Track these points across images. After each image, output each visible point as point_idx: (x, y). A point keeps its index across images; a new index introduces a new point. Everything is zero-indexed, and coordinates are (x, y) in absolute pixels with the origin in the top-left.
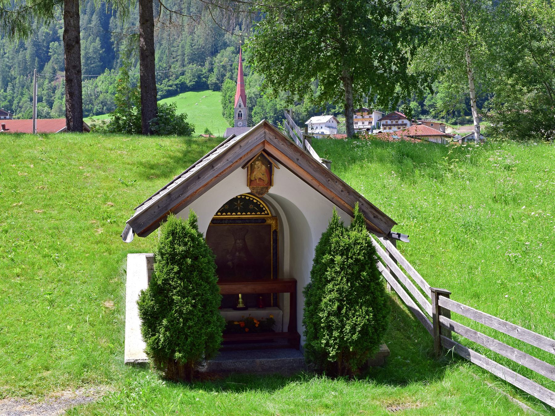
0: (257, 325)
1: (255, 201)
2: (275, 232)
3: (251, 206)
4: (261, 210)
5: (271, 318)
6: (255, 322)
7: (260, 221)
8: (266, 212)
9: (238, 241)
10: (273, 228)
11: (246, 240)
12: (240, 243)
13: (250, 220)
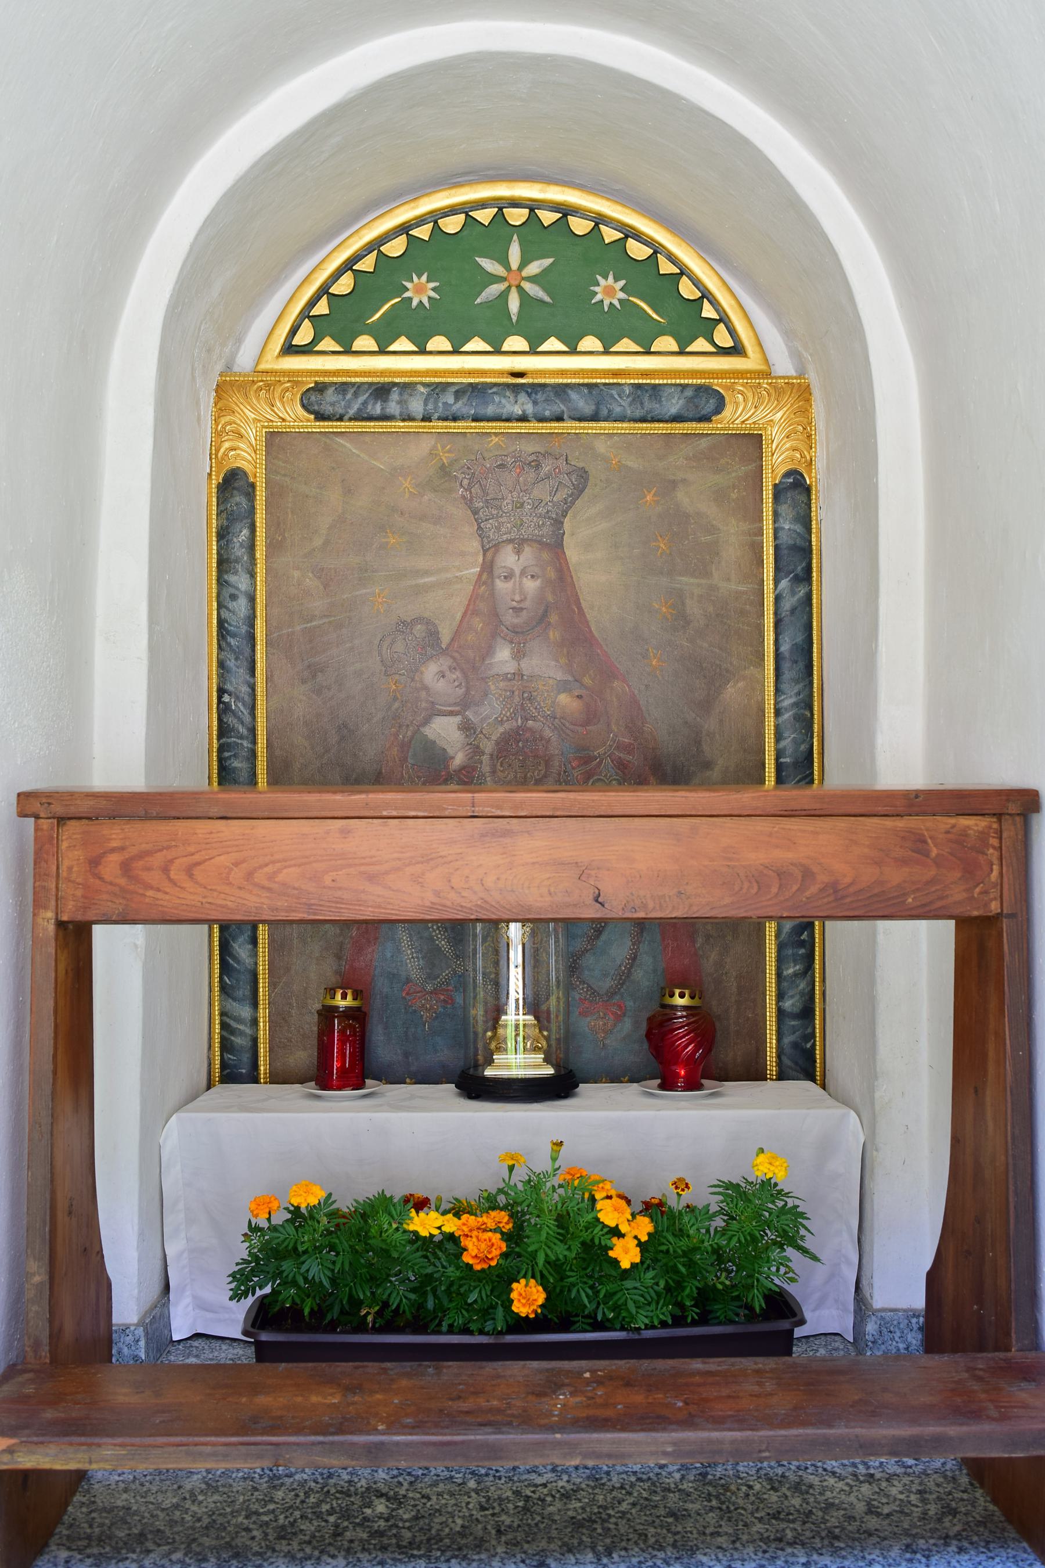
0: (626, 1254)
1: (638, 251)
2: (796, 487)
3: (609, 291)
4: (691, 321)
5: (767, 1185)
6: (609, 1214)
7: (674, 405)
8: (722, 338)
9: (508, 559)
10: (776, 463)
11: (572, 554)
12: (520, 575)
13: (597, 399)
